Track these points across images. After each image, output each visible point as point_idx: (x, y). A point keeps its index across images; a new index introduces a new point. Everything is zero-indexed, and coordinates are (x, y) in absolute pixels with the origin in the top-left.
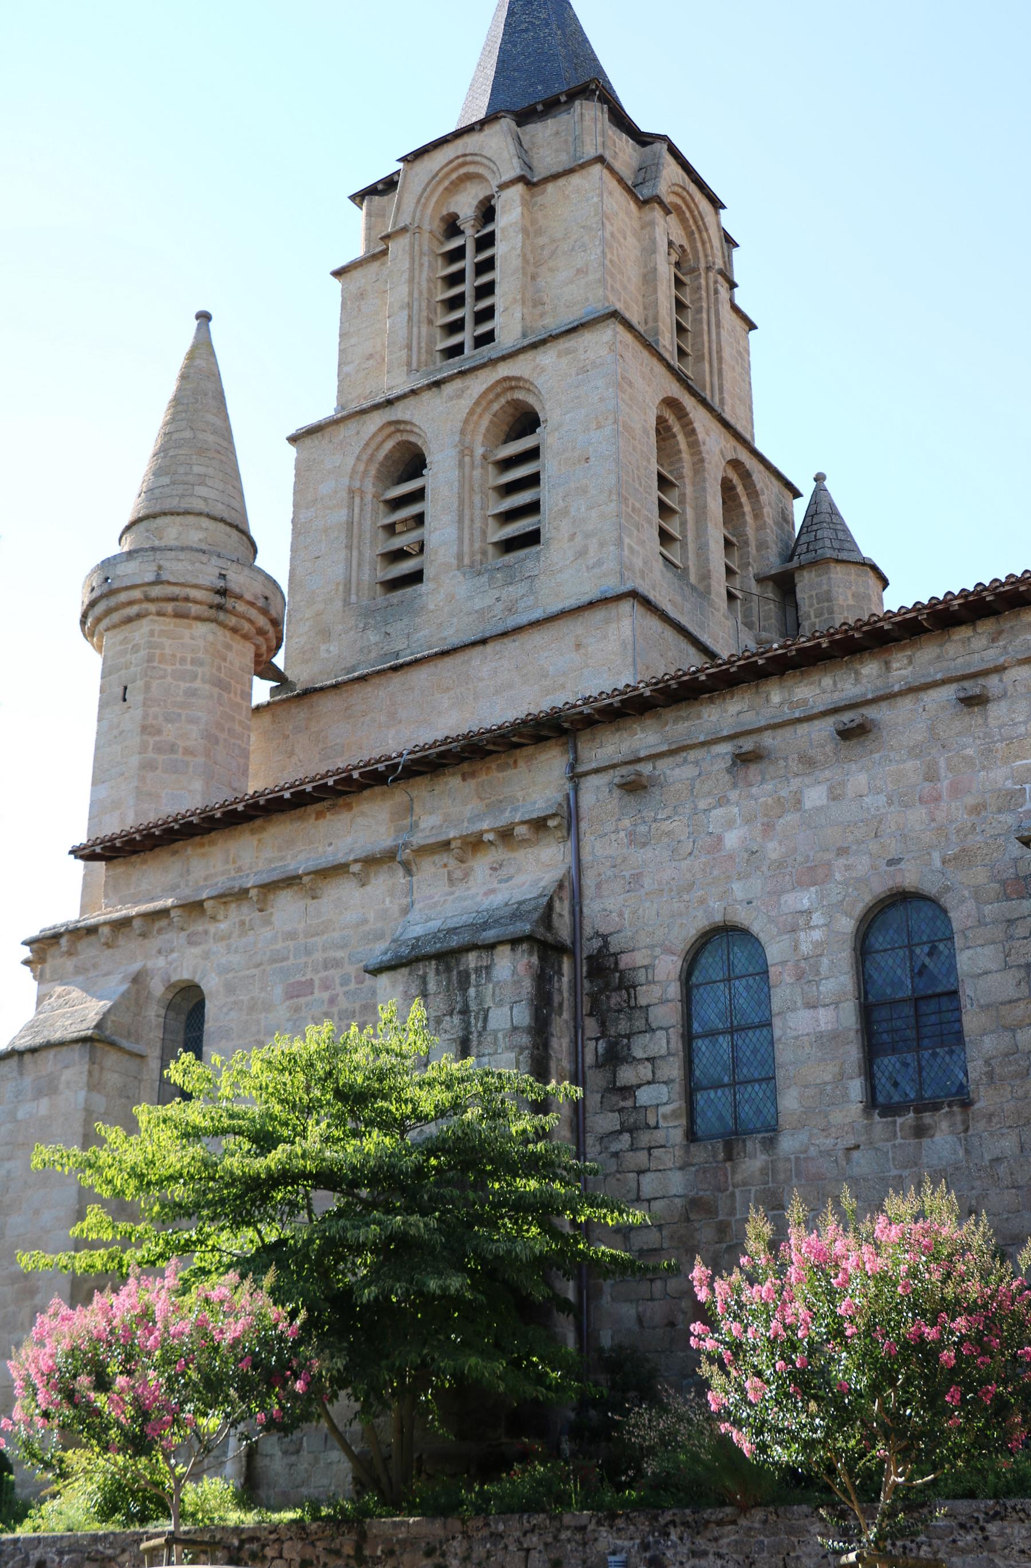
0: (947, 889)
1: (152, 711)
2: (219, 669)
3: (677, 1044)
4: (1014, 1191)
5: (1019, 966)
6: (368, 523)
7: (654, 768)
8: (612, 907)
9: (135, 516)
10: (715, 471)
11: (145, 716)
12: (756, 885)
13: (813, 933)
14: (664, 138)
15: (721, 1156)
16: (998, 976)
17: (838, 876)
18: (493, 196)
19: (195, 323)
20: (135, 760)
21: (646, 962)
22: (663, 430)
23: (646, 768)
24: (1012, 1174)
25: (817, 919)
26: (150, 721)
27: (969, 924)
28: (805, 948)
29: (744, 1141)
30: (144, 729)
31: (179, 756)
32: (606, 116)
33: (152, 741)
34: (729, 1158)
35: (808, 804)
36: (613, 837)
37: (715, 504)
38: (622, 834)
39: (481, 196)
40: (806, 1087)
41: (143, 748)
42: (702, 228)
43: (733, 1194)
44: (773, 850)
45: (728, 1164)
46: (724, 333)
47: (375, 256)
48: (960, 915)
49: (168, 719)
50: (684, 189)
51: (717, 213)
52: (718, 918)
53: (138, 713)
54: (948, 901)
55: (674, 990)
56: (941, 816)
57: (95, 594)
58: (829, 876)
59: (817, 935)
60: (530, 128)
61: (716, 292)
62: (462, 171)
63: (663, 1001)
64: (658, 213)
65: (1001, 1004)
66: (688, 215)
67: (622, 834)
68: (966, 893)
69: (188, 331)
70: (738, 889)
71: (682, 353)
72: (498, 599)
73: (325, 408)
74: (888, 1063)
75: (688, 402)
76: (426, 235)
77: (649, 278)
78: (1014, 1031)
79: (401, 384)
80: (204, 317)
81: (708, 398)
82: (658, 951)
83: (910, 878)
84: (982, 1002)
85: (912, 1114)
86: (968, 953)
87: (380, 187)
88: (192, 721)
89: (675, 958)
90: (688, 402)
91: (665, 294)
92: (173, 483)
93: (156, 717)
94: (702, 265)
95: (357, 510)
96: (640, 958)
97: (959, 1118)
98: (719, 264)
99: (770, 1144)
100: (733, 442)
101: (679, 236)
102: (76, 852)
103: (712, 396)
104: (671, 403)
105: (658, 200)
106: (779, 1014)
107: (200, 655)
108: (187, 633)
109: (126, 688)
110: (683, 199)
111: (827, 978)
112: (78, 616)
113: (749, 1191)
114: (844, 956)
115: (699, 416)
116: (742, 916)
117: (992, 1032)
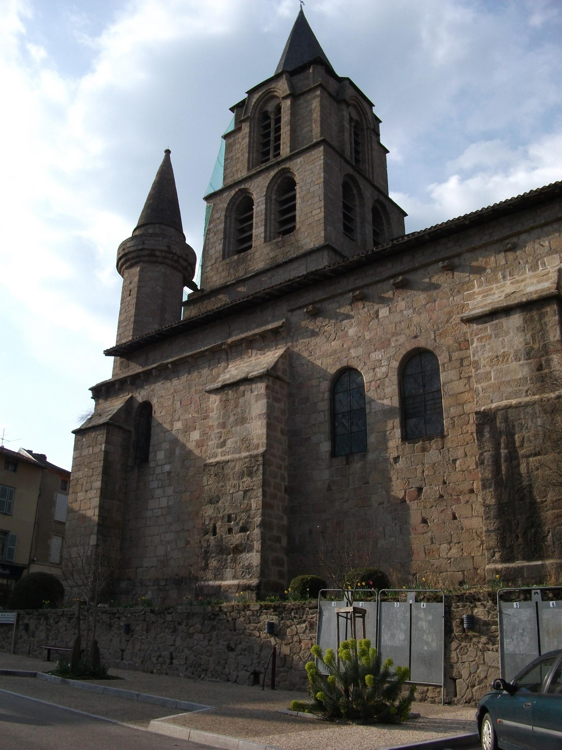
0: (436, 347)
3: (327, 417)
4: (461, 472)
5: (465, 378)
7: (322, 305)
8: (304, 363)
10: (369, 204)
12: (360, 351)
13: (382, 368)
14: (348, 79)
15: (344, 463)
16: (457, 382)
17: (393, 344)
18: (281, 103)
19: (164, 154)
21: (316, 384)
22: (345, 185)
23: (318, 306)
24: (461, 465)
25: (384, 363)
27: (446, 361)
28: (379, 375)
29: (353, 456)
32: (324, 71)
34: (347, 463)
35: (380, 316)
36: (305, 334)
37: (369, 217)
38: (309, 333)
39: (275, 104)
40: (379, 432)
42: (365, 114)
43: (349, 478)
44: (368, 336)
45: (347, 466)
46: (374, 153)
47: (238, 130)
48: (442, 358)
50: (357, 98)
51: (372, 109)
52: (345, 364)
54: (437, 352)
55: (327, 395)
56: (434, 317)
57: (120, 255)
58: (389, 344)
59: (384, 369)
60: (295, 77)
61: (371, 137)
63: (323, 400)
64: (344, 107)
65: (458, 394)
66: (359, 108)
67: (309, 333)
68: (444, 348)
70: (353, 352)
71: (357, 161)
73: (219, 185)
74: (412, 422)
75: (357, 176)
76: (256, 120)
77: (341, 130)
78: (463, 405)
79: (244, 174)
80: (168, 152)
81: (368, 176)
82: (321, 379)
83: (422, 343)
84: (450, 393)
85: (421, 442)
86: (445, 373)
87: (240, 104)
89: (328, 382)
90: (357, 176)
91: (347, 136)
94: (365, 127)
95: (228, 224)
96: (314, 382)
97: (440, 443)
98: (372, 127)
99: (364, 456)
100: (376, 193)
101: (355, 116)
102: (108, 353)
103: (369, 176)
104: (349, 176)
105: (344, 101)
106: (368, 403)
110: (357, 102)
111: (388, 387)
113: (355, 477)
114: (395, 378)
115: (362, 184)
116: (354, 364)
117: (454, 406)
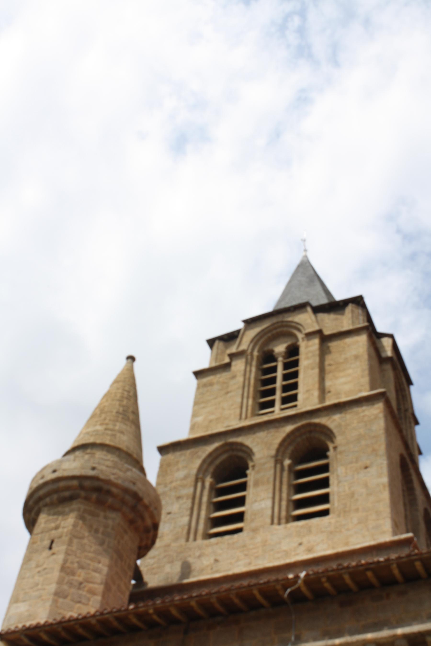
1: (71, 558)
2: (119, 542)
6: (205, 499)
9: (76, 444)
11: (65, 561)
20: (53, 587)
26: (68, 564)
30: (63, 569)
31: (84, 593)
33: (67, 579)
41: (60, 582)
49: (82, 567)
53: (60, 557)
62: (279, 330)
69: (123, 363)
72: (300, 544)
80: (132, 358)
87: (226, 337)
88: (96, 570)
92: (106, 429)
93: (72, 563)
107: (109, 530)
108: (102, 514)
109: (52, 542)
112: (68, 447)
